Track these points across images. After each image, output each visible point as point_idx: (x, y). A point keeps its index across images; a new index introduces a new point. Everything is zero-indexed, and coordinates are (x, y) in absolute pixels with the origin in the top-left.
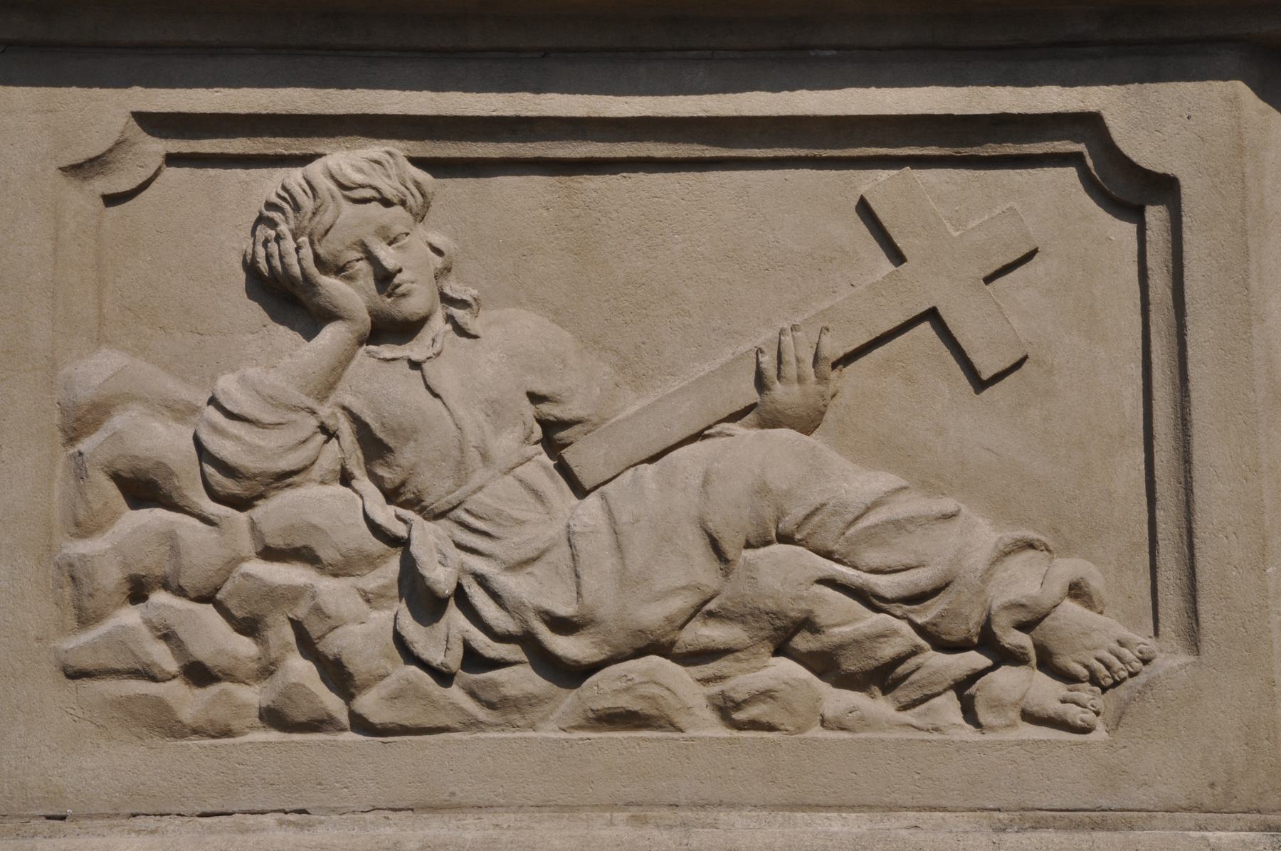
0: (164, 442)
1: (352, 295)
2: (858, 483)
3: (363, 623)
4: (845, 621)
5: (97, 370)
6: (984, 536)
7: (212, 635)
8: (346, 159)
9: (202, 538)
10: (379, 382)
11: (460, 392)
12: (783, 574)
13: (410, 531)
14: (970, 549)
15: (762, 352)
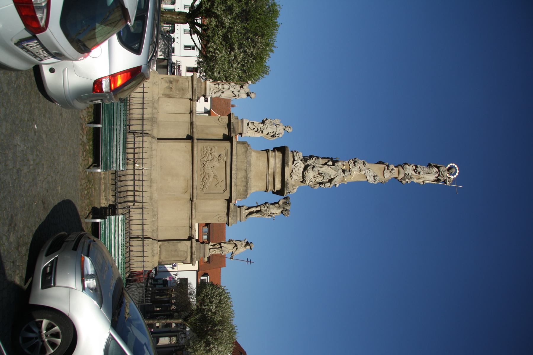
0: (213, 150)
1: (220, 158)
2: (211, 180)
3: (205, 159)
4: (205, 179)
5: (216, 148)
6: (209, 185)
7: (205, 152)
8: (225, 158)
9: (209, 152)
10: (216, 159)
11: (216, 163)
12: (207, 176)
13: (105, 77)
14: (208, 184)
15: (302, 182)
